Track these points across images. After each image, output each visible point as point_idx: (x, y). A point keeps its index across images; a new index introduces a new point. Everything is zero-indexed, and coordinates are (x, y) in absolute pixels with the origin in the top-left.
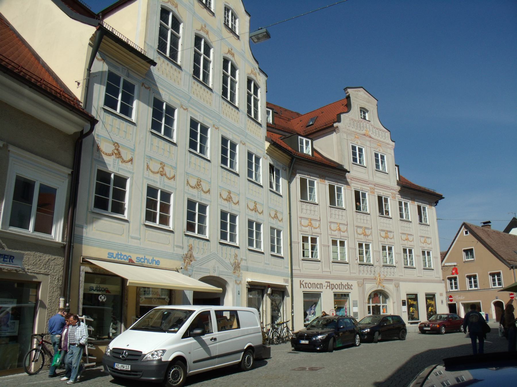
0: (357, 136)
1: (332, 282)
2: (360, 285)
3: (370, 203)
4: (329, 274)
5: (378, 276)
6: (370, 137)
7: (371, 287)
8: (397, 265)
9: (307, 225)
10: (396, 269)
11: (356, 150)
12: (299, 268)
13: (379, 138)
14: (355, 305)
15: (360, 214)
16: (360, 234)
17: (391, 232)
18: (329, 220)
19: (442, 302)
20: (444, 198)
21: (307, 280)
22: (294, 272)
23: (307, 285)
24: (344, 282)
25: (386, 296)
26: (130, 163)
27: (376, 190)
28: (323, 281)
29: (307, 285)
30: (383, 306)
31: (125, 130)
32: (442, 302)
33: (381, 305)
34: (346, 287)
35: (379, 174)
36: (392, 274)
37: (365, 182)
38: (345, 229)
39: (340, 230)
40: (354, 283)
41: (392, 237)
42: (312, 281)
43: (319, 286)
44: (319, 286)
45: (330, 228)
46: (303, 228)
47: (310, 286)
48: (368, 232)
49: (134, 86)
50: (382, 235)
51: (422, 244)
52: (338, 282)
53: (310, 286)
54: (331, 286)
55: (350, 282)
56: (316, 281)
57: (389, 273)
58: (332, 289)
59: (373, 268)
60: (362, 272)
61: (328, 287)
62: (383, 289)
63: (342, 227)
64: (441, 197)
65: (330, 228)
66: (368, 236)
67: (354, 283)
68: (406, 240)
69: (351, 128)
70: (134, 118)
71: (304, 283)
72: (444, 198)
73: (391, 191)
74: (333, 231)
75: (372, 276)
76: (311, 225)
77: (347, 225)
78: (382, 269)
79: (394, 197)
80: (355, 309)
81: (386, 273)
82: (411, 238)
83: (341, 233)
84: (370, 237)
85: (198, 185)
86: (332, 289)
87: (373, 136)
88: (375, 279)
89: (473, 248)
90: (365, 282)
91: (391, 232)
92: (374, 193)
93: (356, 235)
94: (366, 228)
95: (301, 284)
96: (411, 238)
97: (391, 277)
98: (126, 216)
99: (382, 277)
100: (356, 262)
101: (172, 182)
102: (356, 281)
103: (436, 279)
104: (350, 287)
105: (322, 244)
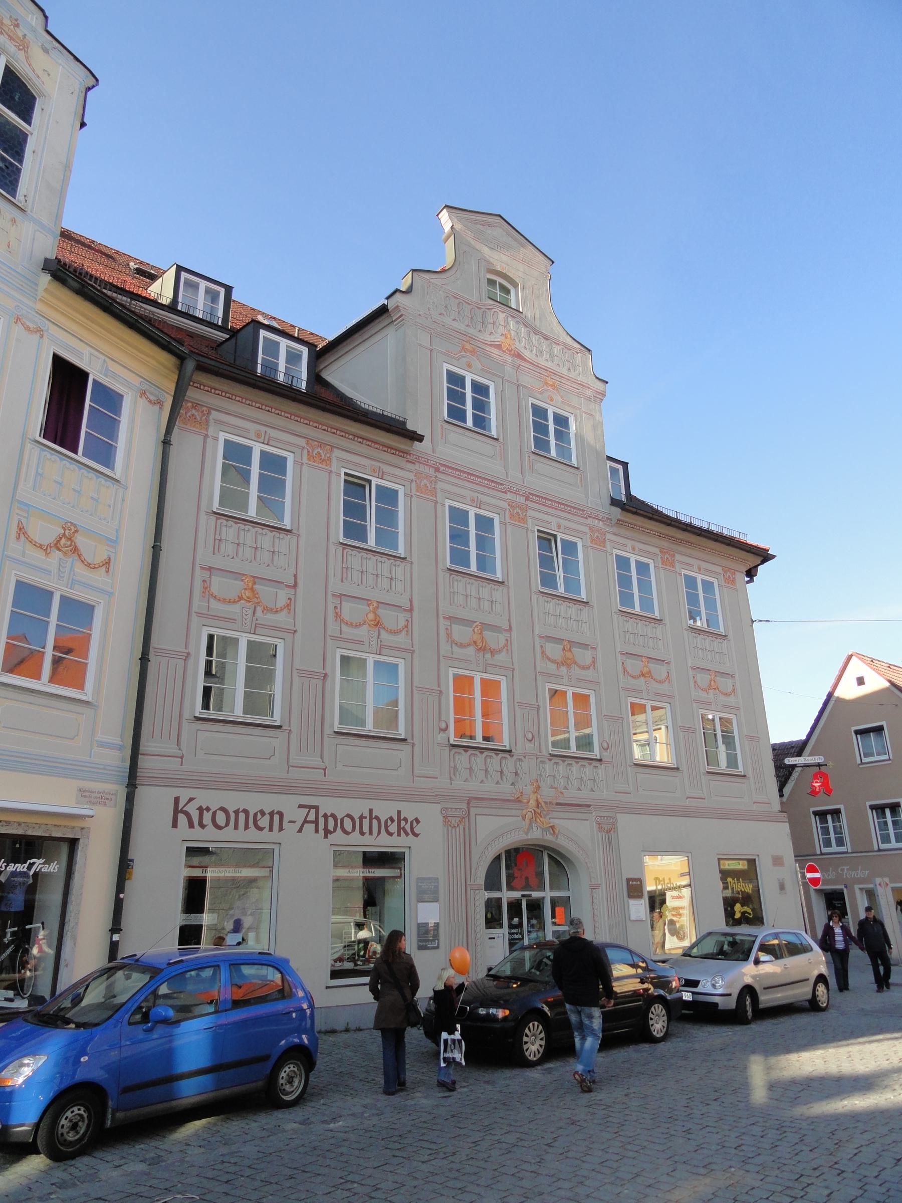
0: (468, 346)
1: (328, 805)
2: (454, 821)
3: (512, 551)
4: (318, 775)
5: (529, 789)
6: (519, 356)
7: (498, 832)
8: (606, 756)
9: (234, 595)
10: (601, 770)
11: (696, 589)
12: (174, 751)
13: (542, 361)
14: (428, 893)
15: (467, 579)
16: (462, 646)
17: (585, 646)
18: (336, 585)
19: (782, 887)
20: (773, 557)
21: (206, 798)
22: (143, 762)
23: (207, 817)
24: (385, 810)
25: (560, 862)
26: (104, 569)
27: (530, 513)
28: (289, 805)
29: (207, 817)
30: (554, 903)
31: (96, 496)
32: (782, 887)
33: (547, 894)
34: (393, 828)
35: (542, 466)
36: (589, 784)
37: (493, 483)
38: (402, 623)
39: (378, 624)
40: (429, 816)
41: (588, 661)
42: (234, 801)
43: (264, 822)
44: (264, 822)
45: (337, 615)
46: (214, 604)
47: (221, 818)
48: (494, 639)
49: (122, 396)
50: (549, 653)
51: (704, 694)
52: (358, 808)
53: (221, 818)
54: (324, 824)
55: (410, 811)
56: (254, 802)
57: (576, 783)
58: (327, 832)
59: (509, 764)
60: (481, 775)
61: (310, 827)
62: (549, 837)
63: (388, 617)
64: (765, 556)
65: (337, 615)
66: (493, 652)
67: (429, 816)
68: (643, 675)
69: (448, 320)
70: (118, 471)
71: (192, 809)
72: (773, 557)
73: (589, 521)
74: (351, 625)
75: (506, 789)
76: (253, 598)
77: (411, 610)
78: (548, 766)
79: (599, 542)
80: (429, 913)
81: (562, 783)
82: (659, 671)
83: (384, 635)
84: (501, 658)
85: (67, 543)
86: (327, 832)
87: (527, 354)
88: (518, 800)
89: (884, 723)
90: (473, 811)
91: (585, 646)
92: (523, 520)
93: (445, 648)
94: (485, 626)
95: (176, 812)
96: (659, 671)
97: (584, 796)
98: (88, 693)
99: (547, 793)
100: (441, 737)
101: (99, 577)
102: (438, 807)
103: (755, 807)
104: (406, 826)
105: (297, 666)
